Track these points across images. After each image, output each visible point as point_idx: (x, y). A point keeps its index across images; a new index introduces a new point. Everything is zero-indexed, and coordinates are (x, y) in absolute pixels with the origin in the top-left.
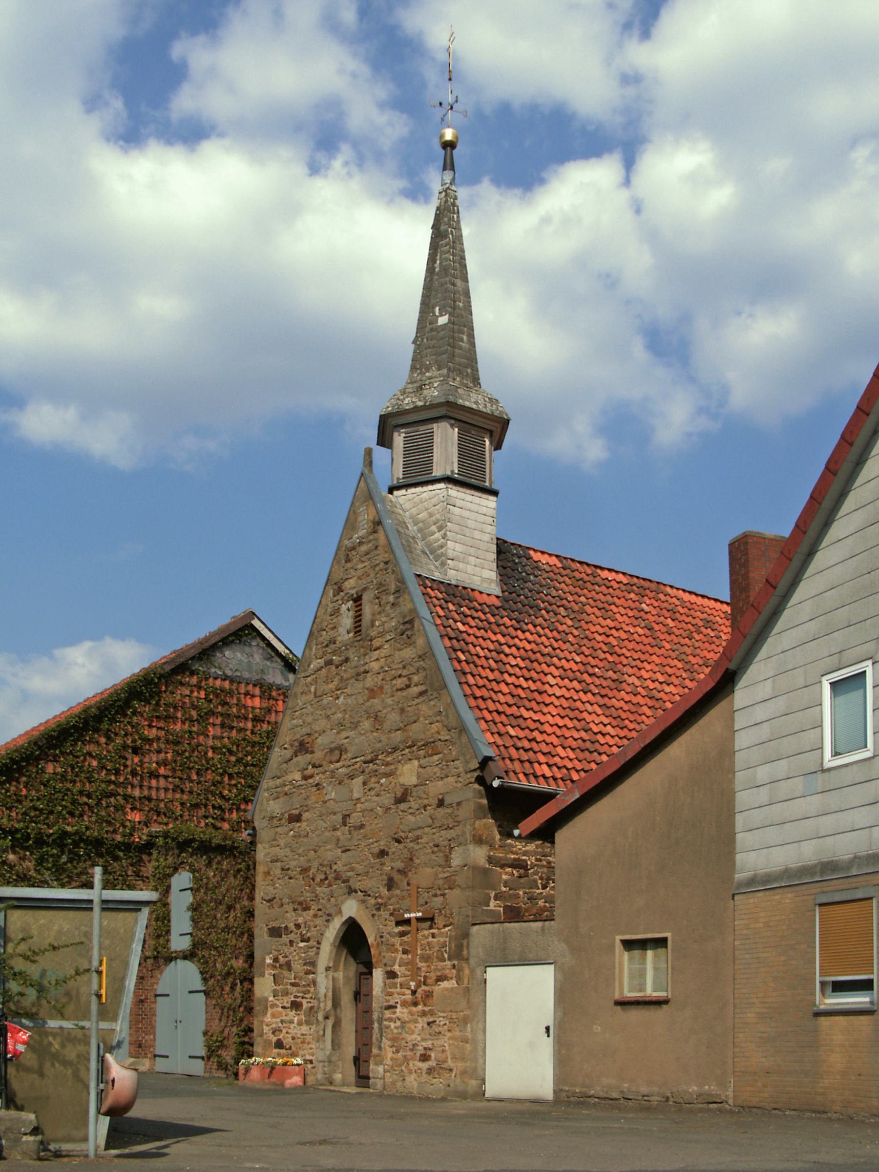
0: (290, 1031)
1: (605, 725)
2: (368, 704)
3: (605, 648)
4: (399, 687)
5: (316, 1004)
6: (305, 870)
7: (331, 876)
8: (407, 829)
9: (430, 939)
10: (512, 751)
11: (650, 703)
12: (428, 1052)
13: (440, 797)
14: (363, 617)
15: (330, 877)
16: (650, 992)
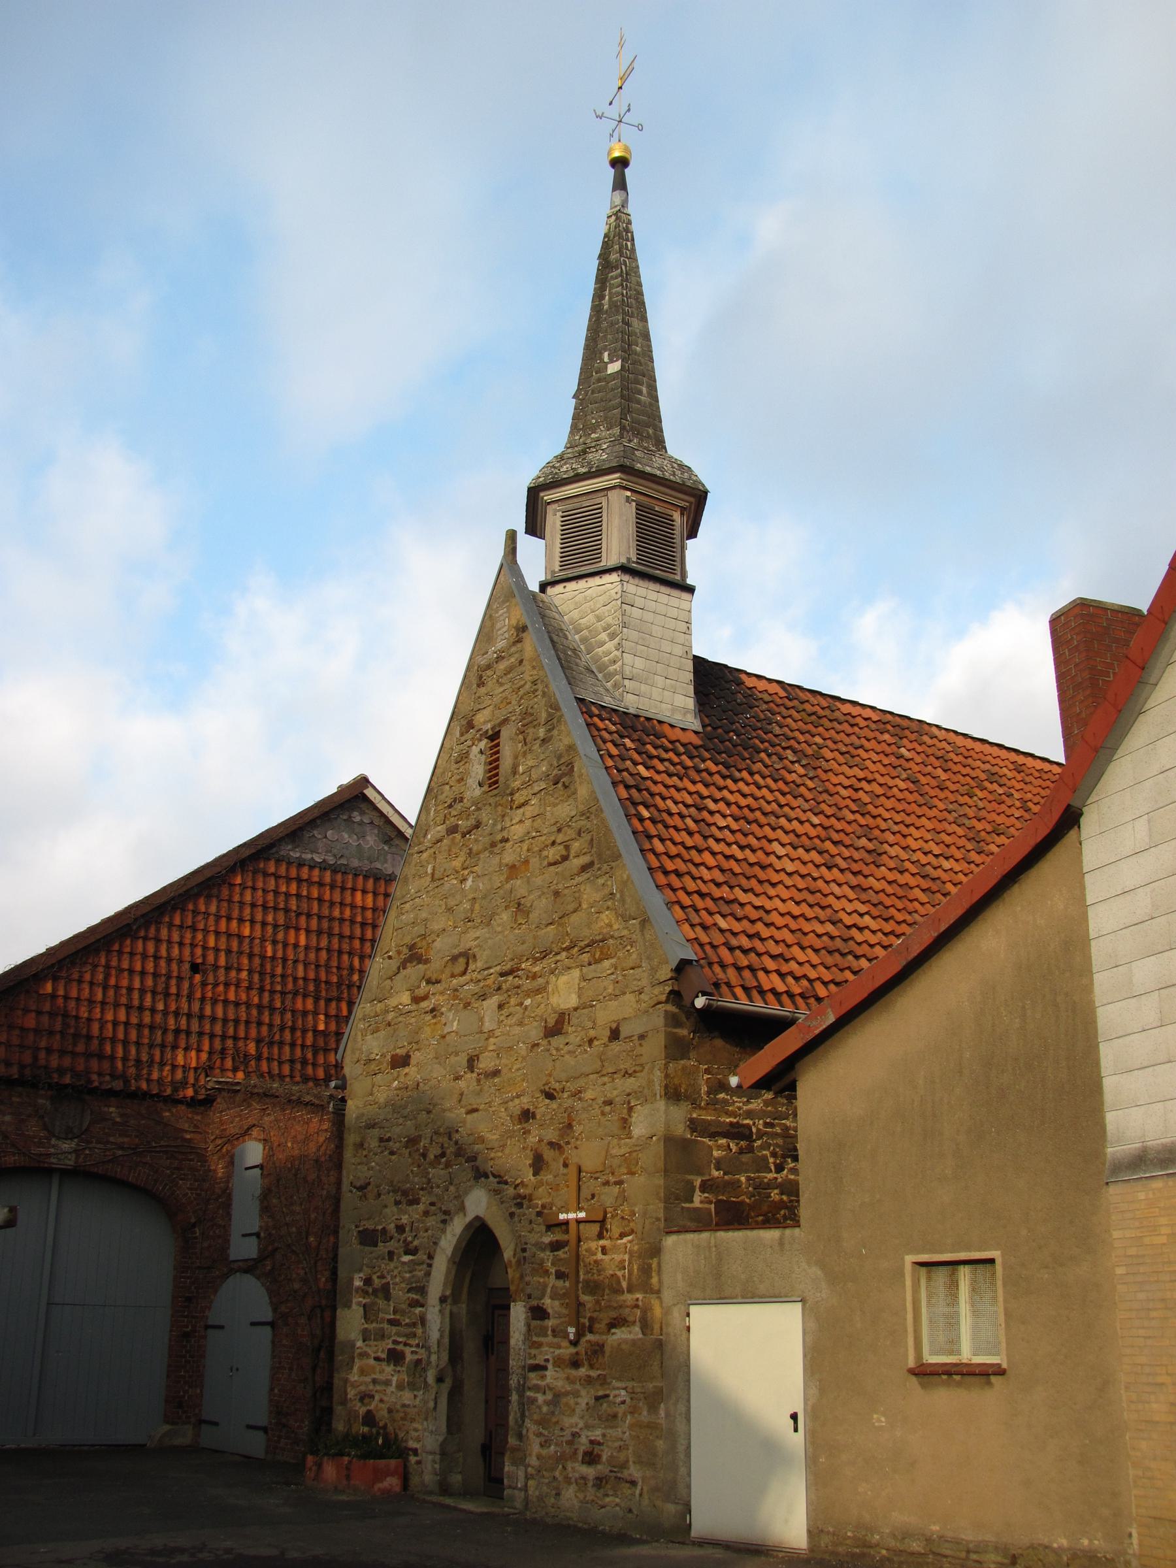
0: (385, 1398)
1: (861, 915)
2: (508, 886)
3: (854, 807)
4: (551, 859)
5: (424, 1356)
6: (412, 1141)
7: (451, 1150)
8: (563, 1076)
9: (600, 1256)
10: (724, 952)
11: (925, 884)
12: (597, 1449)
13: (614, 1026)
14: (501, 762)
15: (448, 1152)
16: (967, 1354)
